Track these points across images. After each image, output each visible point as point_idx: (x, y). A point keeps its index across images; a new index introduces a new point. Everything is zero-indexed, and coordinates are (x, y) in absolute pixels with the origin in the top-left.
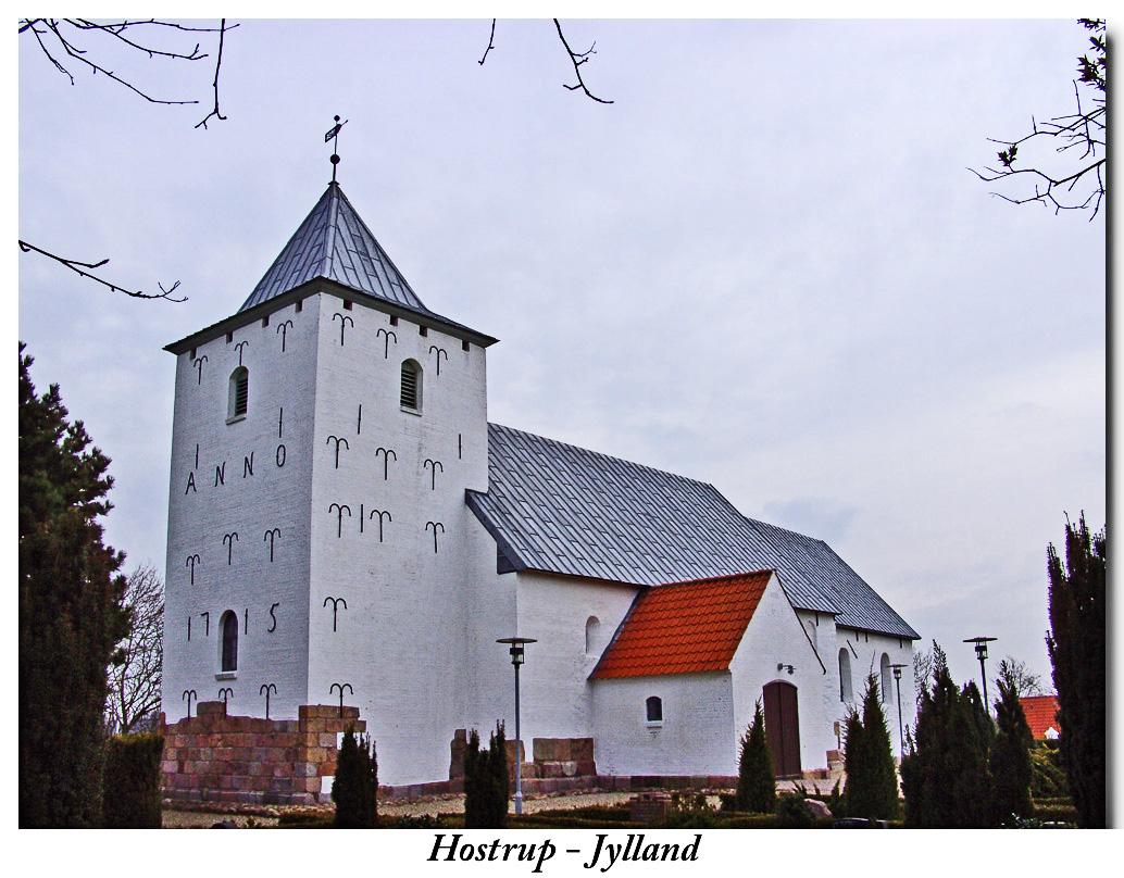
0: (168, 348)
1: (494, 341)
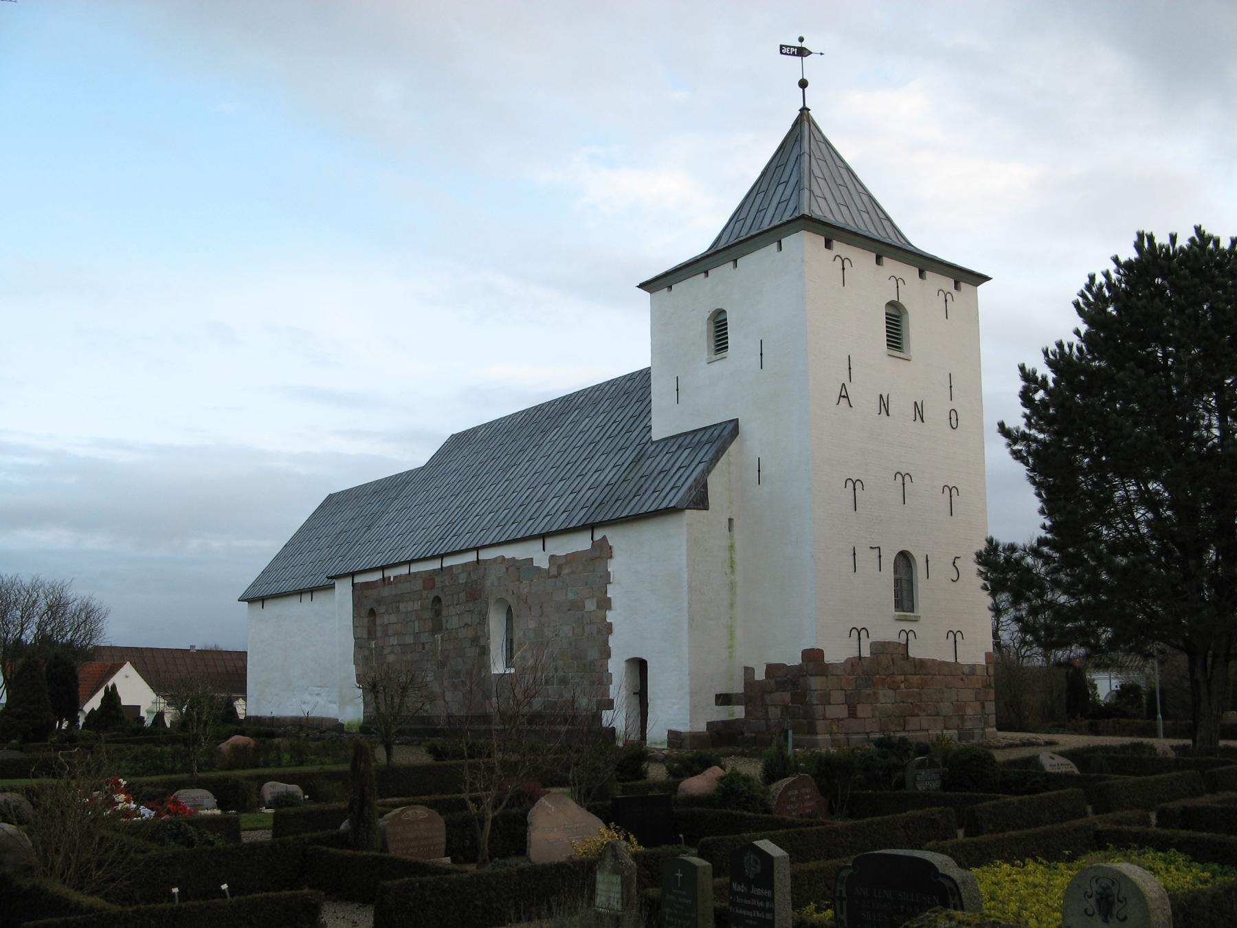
0: (641, 286)
1: (986, 279)
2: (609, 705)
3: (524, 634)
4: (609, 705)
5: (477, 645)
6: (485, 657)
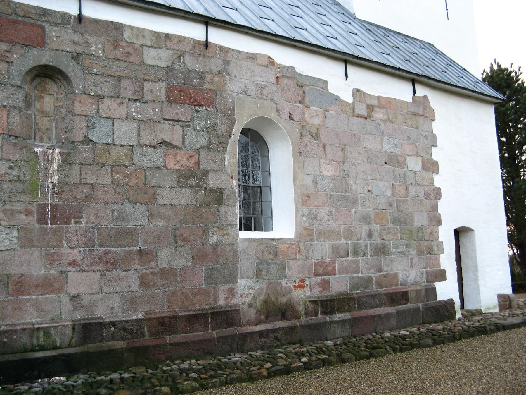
2: (442, 276)
3: (315, 182)
4: (442, 276)
5: (198, 185)
6: (223, 209)
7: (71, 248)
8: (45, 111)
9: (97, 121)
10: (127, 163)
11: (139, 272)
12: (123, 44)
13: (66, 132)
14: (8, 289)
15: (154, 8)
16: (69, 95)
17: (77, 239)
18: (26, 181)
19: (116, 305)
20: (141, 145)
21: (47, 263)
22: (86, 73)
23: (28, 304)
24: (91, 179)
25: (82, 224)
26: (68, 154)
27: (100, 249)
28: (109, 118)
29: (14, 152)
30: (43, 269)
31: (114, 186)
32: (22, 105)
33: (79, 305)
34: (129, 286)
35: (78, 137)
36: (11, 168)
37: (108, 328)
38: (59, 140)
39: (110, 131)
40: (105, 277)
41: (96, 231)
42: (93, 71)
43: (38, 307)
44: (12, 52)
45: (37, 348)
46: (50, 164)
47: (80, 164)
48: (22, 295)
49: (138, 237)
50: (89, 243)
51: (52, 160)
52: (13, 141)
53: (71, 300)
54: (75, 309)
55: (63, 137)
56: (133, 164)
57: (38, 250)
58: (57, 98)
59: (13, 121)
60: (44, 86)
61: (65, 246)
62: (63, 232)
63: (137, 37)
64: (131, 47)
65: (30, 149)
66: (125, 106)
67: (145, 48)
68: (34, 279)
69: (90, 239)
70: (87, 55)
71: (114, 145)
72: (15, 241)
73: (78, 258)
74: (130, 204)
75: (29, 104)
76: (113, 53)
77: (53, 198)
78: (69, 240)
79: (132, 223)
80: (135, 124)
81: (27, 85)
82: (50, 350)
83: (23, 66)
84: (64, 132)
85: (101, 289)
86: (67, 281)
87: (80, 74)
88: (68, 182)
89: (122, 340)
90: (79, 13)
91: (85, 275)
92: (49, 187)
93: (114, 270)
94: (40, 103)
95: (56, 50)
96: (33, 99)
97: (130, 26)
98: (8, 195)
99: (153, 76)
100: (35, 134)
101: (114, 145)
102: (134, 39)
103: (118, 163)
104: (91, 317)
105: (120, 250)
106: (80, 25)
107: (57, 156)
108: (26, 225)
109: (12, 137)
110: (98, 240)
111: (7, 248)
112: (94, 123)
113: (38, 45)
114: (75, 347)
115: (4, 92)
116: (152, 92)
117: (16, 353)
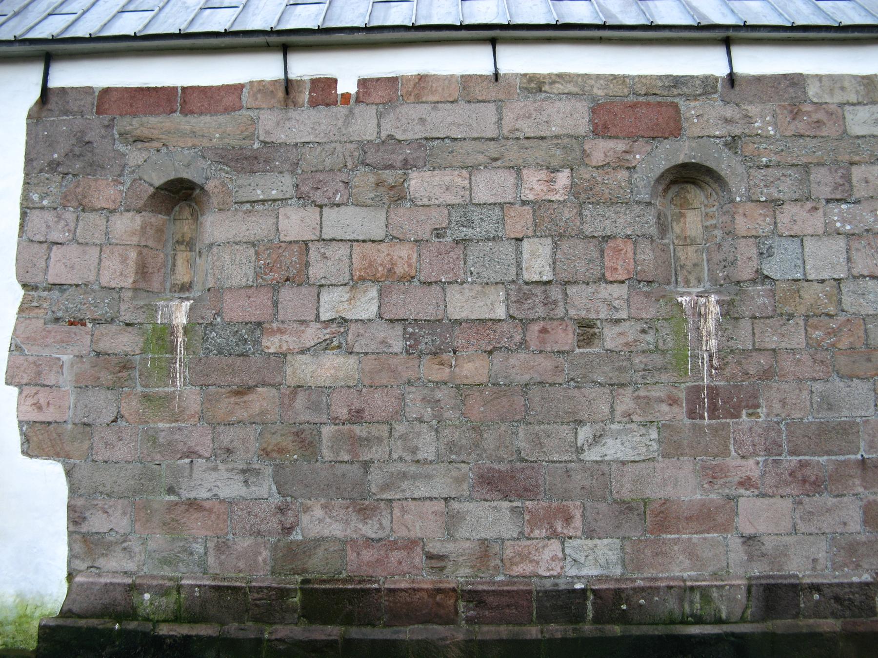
7: (743, 457)
8: (689, 236)
9: (776, 244)
10: (832, 310)
11: (861, 499)
12: (807, 108)
13: (725, 267)
14: (645, 522)
15: (856, 35)
16: (726, 206)
17: (753, 441)
18: (667, 350)
19: (821, 555)
20: (855, 277)
21: (704, 482)
22: (750, 167)
23: (676, 548)
24: (772, 341)
25: (760, 417)
26: (731, 303)
27: (791, 458)
28: (795, 236)
29: (646, 307)
30: (698, 491)
31: (812, 351)
32: (654, 231)
33: (756, 553)
34: (845, 524)
35: (746, 273)
36: (644, 331)
37: (808, 594)
38: (714, 280)
39: (799, 259)
40: (801, 507)
41: (783, 429)
42: (762, 162)
43: (692, 554)
44: (633, 151)
45: (690, 619)
46: (703, 320)
47: (751, 318)
48: (666, 533)
49: (858, 437)
50: (772, 449)
51: (705, 314)
52: (645, 289)
53: (744, 543)
54: (751, 558)
55: (721, 275)
56: (843, 311)
57: (689, 461)
58: (707, 214)
59: (643, 257)
60: (685, 197)
61: (733, 453)
62: (729, 431)
63: (831, 92)
64: (822, 111)
65: (671, 300)
66: (820, 212)
67: (847, 108)
68: (684, 508)
69: (775, 442)
70: (749, 136)
71: (807, 281)
72: (655, 446)
73: (755, 474)
74: (841, 381)
75: (663, 228)
76: (792, 126)
77: (711, 375)
78: (739, 444)
79: (846, 412)
80: (841, 242)
81: (659, 199)
82: (710, 623)
83: (652, 170)
84: (722, 267)
85: (795, 526)
86: (737, 512)
87: (740, 169)
88: (734, 348)
89: (833, 618)
90: (728, 72)
91: (767, 502)
92: (703, 358)
93: (817, 495)
94: (681, 224)
95: (699, 137)
96: (669, 220)
97: (817, 75)
98: (640, 373)
99: (866, 156)
100: (676, 274)
101: (807, 281)
102: (826, 96)
103: (817, 311)
104: (778, 573)
105: (827, 460)
106: (732, 91)
107: (713, 307)
108: (670, 420)
109: (642, 283)
110: (788, 442)
111: (642, 458)
112: (770, 247)
113: (671, 134)
114: (752, 622)
115: (626, 215)
116: (867, 182)
117: (657, 624)
